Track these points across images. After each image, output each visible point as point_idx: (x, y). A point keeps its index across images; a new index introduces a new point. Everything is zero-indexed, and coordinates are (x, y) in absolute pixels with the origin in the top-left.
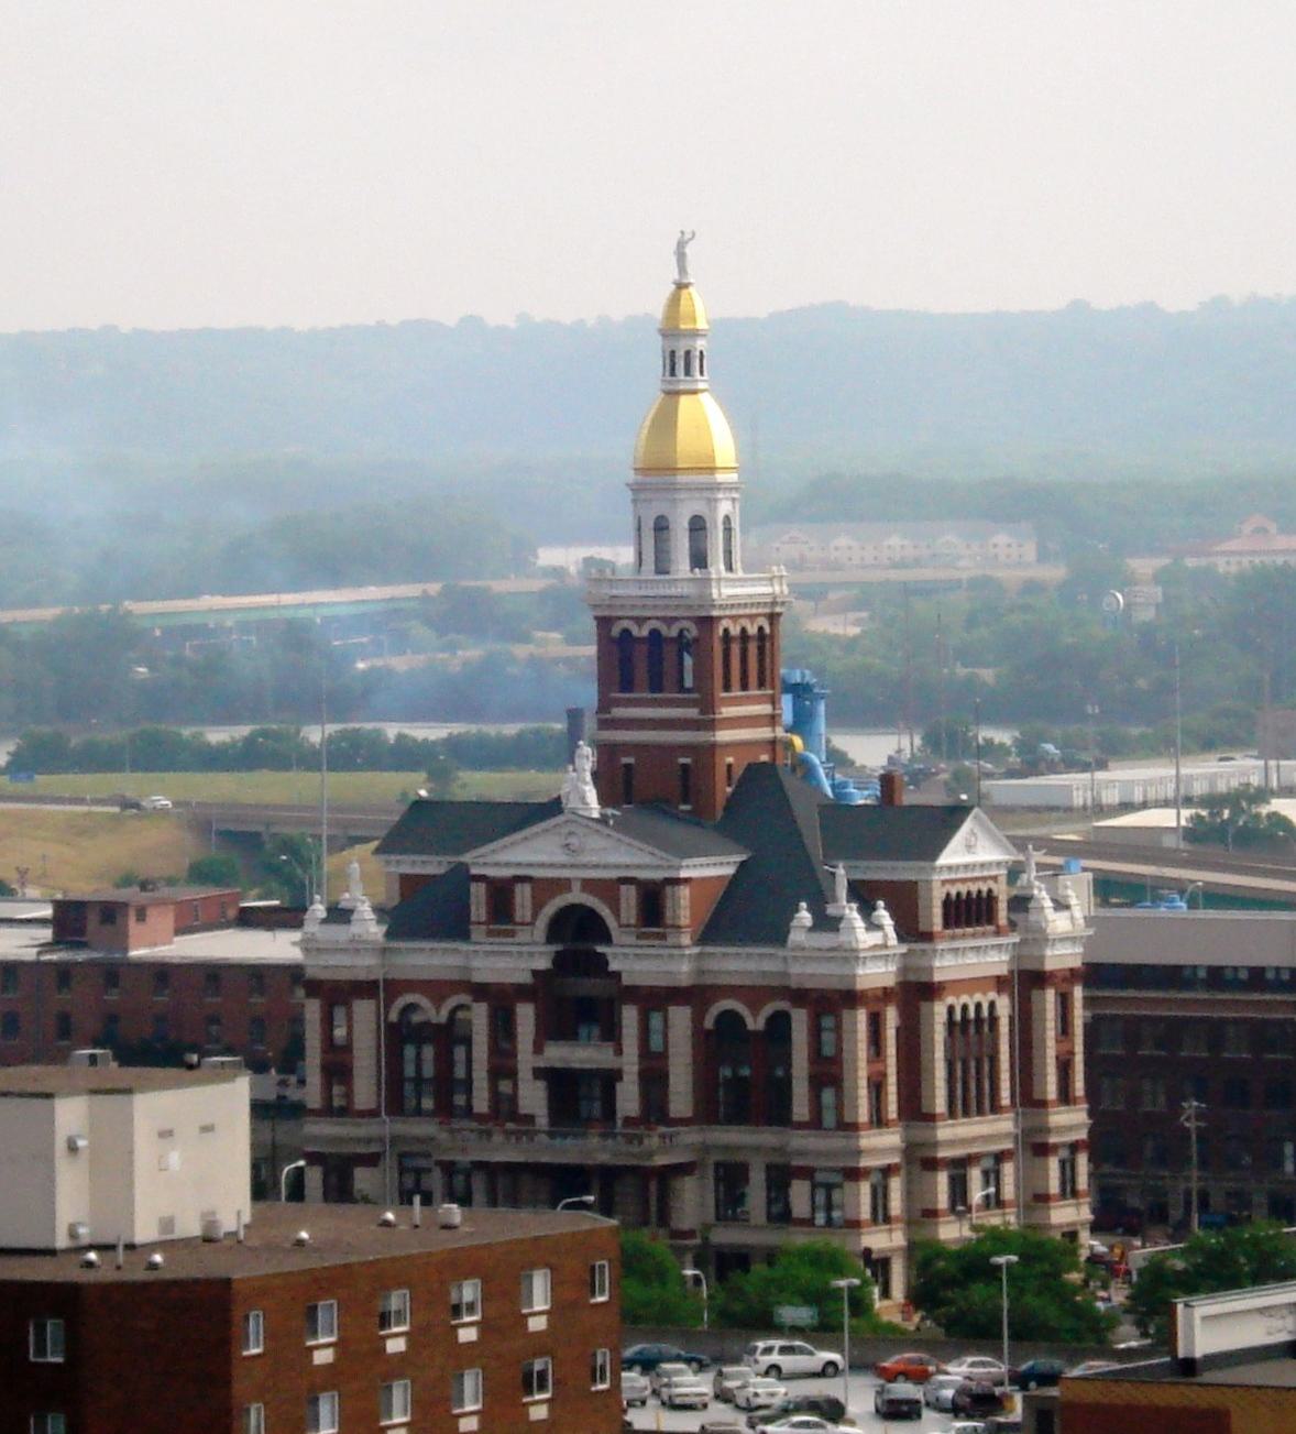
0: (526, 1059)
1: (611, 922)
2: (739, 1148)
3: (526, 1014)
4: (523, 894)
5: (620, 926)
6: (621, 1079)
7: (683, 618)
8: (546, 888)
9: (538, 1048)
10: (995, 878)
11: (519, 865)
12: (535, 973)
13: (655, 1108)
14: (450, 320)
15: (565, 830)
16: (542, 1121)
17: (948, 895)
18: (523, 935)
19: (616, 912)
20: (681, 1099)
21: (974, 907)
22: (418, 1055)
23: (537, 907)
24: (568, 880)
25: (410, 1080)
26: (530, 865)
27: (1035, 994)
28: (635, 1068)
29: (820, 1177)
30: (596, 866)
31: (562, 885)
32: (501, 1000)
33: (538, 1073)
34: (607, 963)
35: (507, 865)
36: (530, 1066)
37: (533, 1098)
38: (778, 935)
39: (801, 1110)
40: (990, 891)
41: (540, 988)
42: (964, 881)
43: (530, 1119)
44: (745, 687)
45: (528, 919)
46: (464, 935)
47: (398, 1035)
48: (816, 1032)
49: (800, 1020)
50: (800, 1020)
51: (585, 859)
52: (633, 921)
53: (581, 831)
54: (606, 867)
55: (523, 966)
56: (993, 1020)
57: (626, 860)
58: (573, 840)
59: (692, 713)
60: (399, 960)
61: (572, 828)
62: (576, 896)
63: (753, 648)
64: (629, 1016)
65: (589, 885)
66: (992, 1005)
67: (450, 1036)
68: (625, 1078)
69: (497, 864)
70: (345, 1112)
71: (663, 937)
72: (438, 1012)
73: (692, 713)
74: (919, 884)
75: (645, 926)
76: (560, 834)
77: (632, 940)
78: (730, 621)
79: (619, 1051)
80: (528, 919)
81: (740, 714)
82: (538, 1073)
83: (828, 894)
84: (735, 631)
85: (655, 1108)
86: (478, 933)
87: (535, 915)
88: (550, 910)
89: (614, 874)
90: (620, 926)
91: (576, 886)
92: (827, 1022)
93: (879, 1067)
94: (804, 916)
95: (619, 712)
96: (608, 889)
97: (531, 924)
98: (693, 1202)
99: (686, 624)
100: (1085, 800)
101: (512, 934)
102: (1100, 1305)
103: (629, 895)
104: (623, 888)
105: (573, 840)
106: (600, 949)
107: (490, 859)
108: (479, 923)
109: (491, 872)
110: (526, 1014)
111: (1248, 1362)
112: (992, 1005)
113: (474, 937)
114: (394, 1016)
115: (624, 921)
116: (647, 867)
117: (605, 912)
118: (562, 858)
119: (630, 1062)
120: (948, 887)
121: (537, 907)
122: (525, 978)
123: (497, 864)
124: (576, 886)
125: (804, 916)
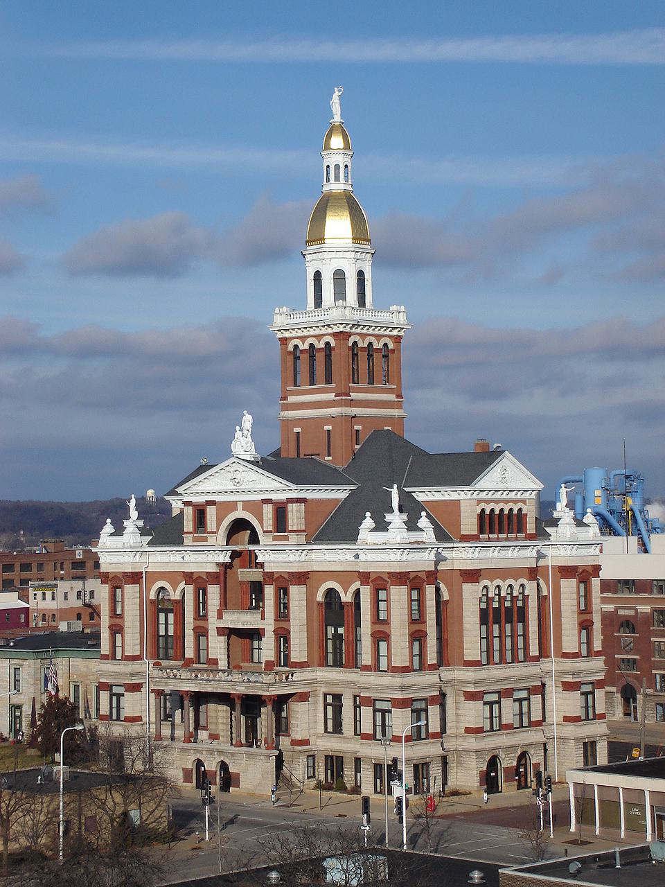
0: (213, 624)
2: (337, 683)
3: (214, 591)
4: (211, 512)
5: (264, 532)
7: (327, 335)
9: (220, 616)
10: (524, 501)
13: (283, 656)
16: (223, 664)
17: (483, 510)
18: (211, 540)
20: (298, 652)
21: (515, 520)
22: (501, 631)
24: (235, 503)
25: (508, 650)
29: (379, 705)
31: (232, 506)
32: (199, 582)
33: (221, 631)
34: (256, 557)
38: (352, 536)
39: (366, 658)
40: (520, 510)
41: (223, 575)
42: (497, 501)
43: (215, 662)
44: (371, 381)
46: (180, 542)
47: (160, 606)
48: (376, 601)
49: (366, 593)
50: (366, 593)
52: (271, 528)
55: (210, 560)
57: (266, 486)
58: (238, 476)
59: (392, 397)
61: (236, 466)
62: (240, 513)
63: (320, 357)
65: (248, 505)
67: (177, 608)
71: (286, 538)
73: (392, 397)
77: (270, 541)
78: (314, 339)
81: (389, 399)
82: (221, 631)
84: (363, 344)
85: (283, 656)
86: (188, 539)
88: (227, 522)
90: (264, 532)
91: (240, 506)
92: (119, 591)
94: (368, 522)
95: (291, 399)
98: (307, 720)
99: (388, 340)
101: (205, 539)
103: (268, 511)
105: (238, 476)
109: (195, 499)
110: (214, 591)
111: (491, 822)
113: (186, 542)
114: (152, 596)
118: (231, 487)
120: (483, 505)
122: (213, 569)
124: (240, 506)
125: (368, 522)
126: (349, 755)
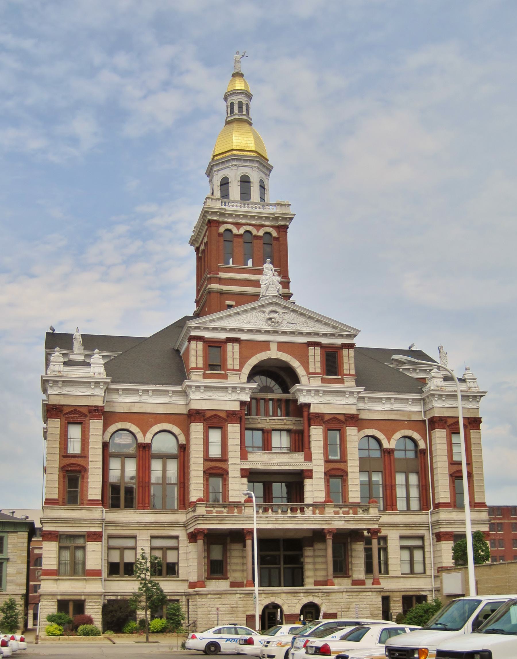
1: (301, 371)
4: (233, 351)
6: (311, 477)
8: (248, 348)
9: (244, 456)
11: (233, 330)
12: (243, 403)
15: (268, 309)
18: (233, 380)
19: (305, 365)
23: (242, 362)
26: (241, 330)
28: (322, 469)
30: (293, 333)
31: (265, 346)
33: (251, 475)
35: (224, 329)
36: (239, 468)
45: (237, 367)
52: (319, 370)
53: (281, 311)
54: (301, 334)
55: (235, 398)
60: (116, 398)
62: (274, 353)
64: (316, 433)
65: (282, 346)
68: (314, 475)
69: (215, 329)
72: (144, 436)
74: (240, 476)
75: (327, 375)
76: (264, 312)
79: (308, 458)
80: (237, 367)
87: (242, 364)
88: (254, 361)
89: (223, 336)
90: (309, 373)
91: (274, 347)
96: (300, 350)
97: (240, 370)
100: (17, 609)
103: (315, 357)
104: (311, 349)
107: (217, 324)
108: (197, 368)
115: (311, 370)
116: (325, 335)
117: (295, 364)
118: (265, 327)
119: (317, 465)
121: (242, 362)
123: (215, 329)
124: (274, 347)
126: (398, 594)
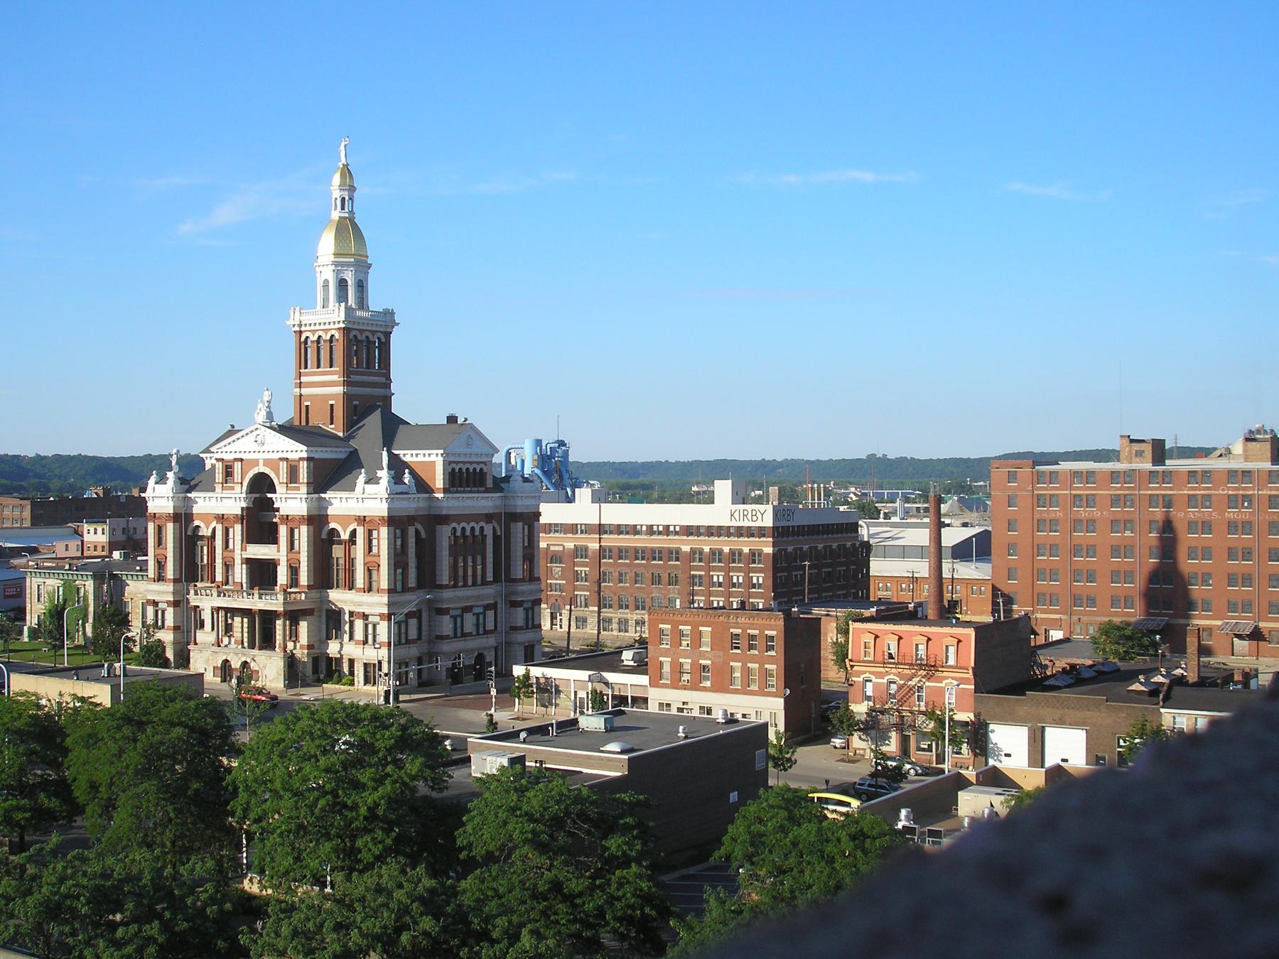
3: (237, 531)
4: (237, 466)
14: (32, 455)
27: (512, 525)
31: (255, 463)
37: (240, 573)
44: (318, 367)
51: (265, 448)
56: (484, 537)
65: (267, 462)
66: (482, 528)
70: (464, 635)
83: (478, 448)
86: (218, 487)
93: (159, 551)
102: (928, 845)
103: (283, 465)
106: (269, 495)
107: (224, 449)
112: (482, 528)
117: (273, 476)
118: (255, 447)
124: (261, 462)
